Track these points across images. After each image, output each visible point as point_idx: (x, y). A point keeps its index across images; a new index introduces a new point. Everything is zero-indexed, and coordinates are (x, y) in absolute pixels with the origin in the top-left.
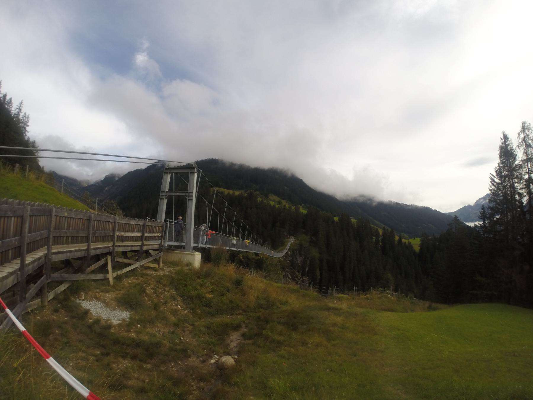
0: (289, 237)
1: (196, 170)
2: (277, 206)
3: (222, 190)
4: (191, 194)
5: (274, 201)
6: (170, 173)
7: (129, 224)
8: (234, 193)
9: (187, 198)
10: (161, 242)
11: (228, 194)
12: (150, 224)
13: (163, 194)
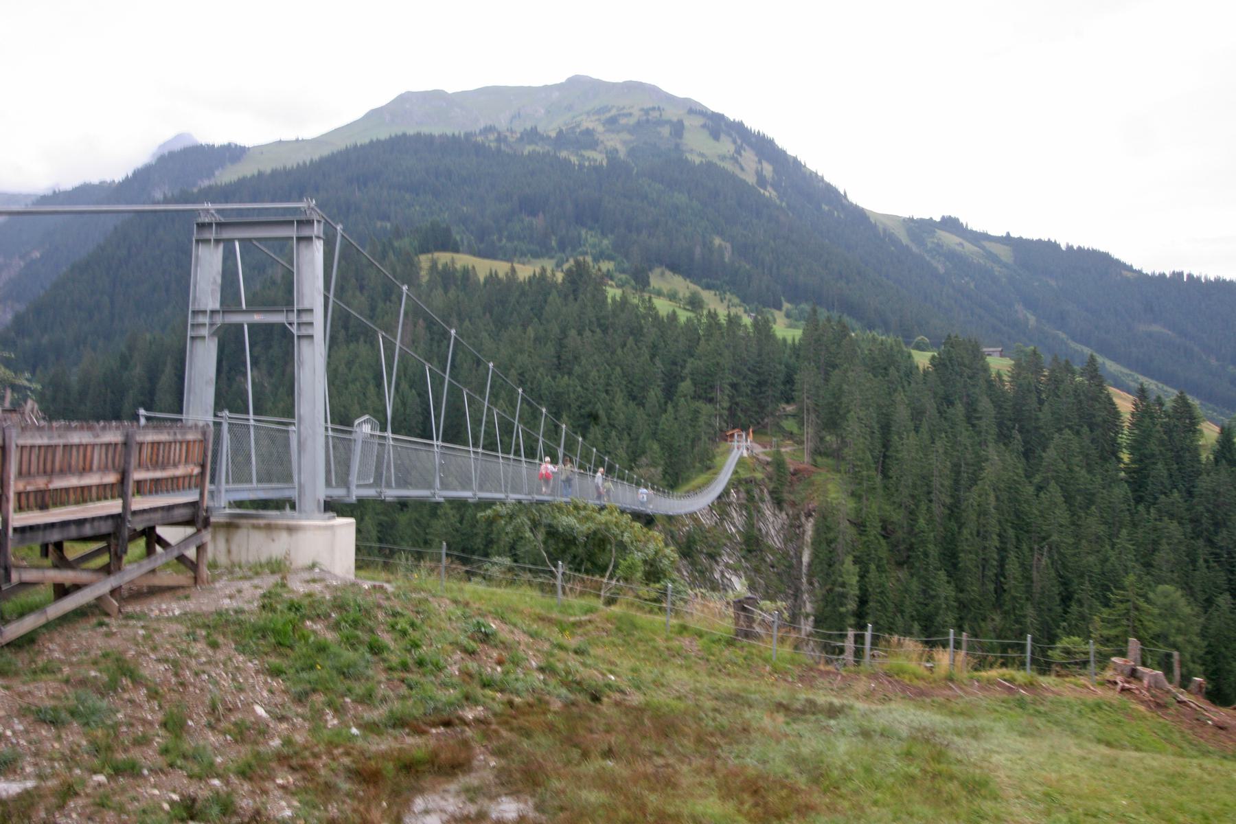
0: (732, 435)
1: (317, 229)
2: (683, 316)
3: (463, 260)
4: (305, 318)
5: (672, 297)
6: (217, 241)
7: (65, 446)
8: (513, 270)
9: (294, 330)
10: (202, 495)
11: (492, 278)
12: (151, 437)
13: (201, 319)
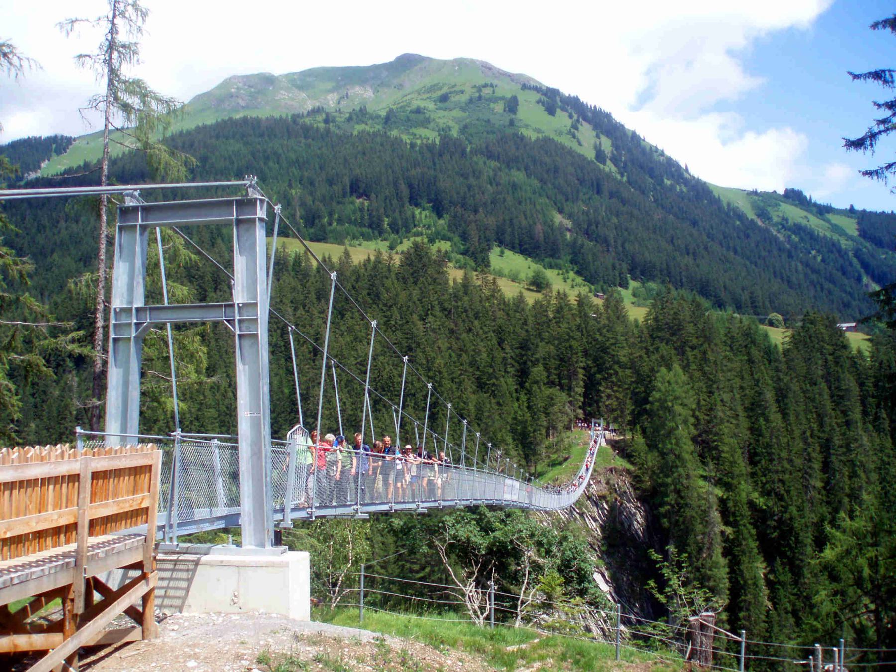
2: (531, 298)
8: (347, 254)
